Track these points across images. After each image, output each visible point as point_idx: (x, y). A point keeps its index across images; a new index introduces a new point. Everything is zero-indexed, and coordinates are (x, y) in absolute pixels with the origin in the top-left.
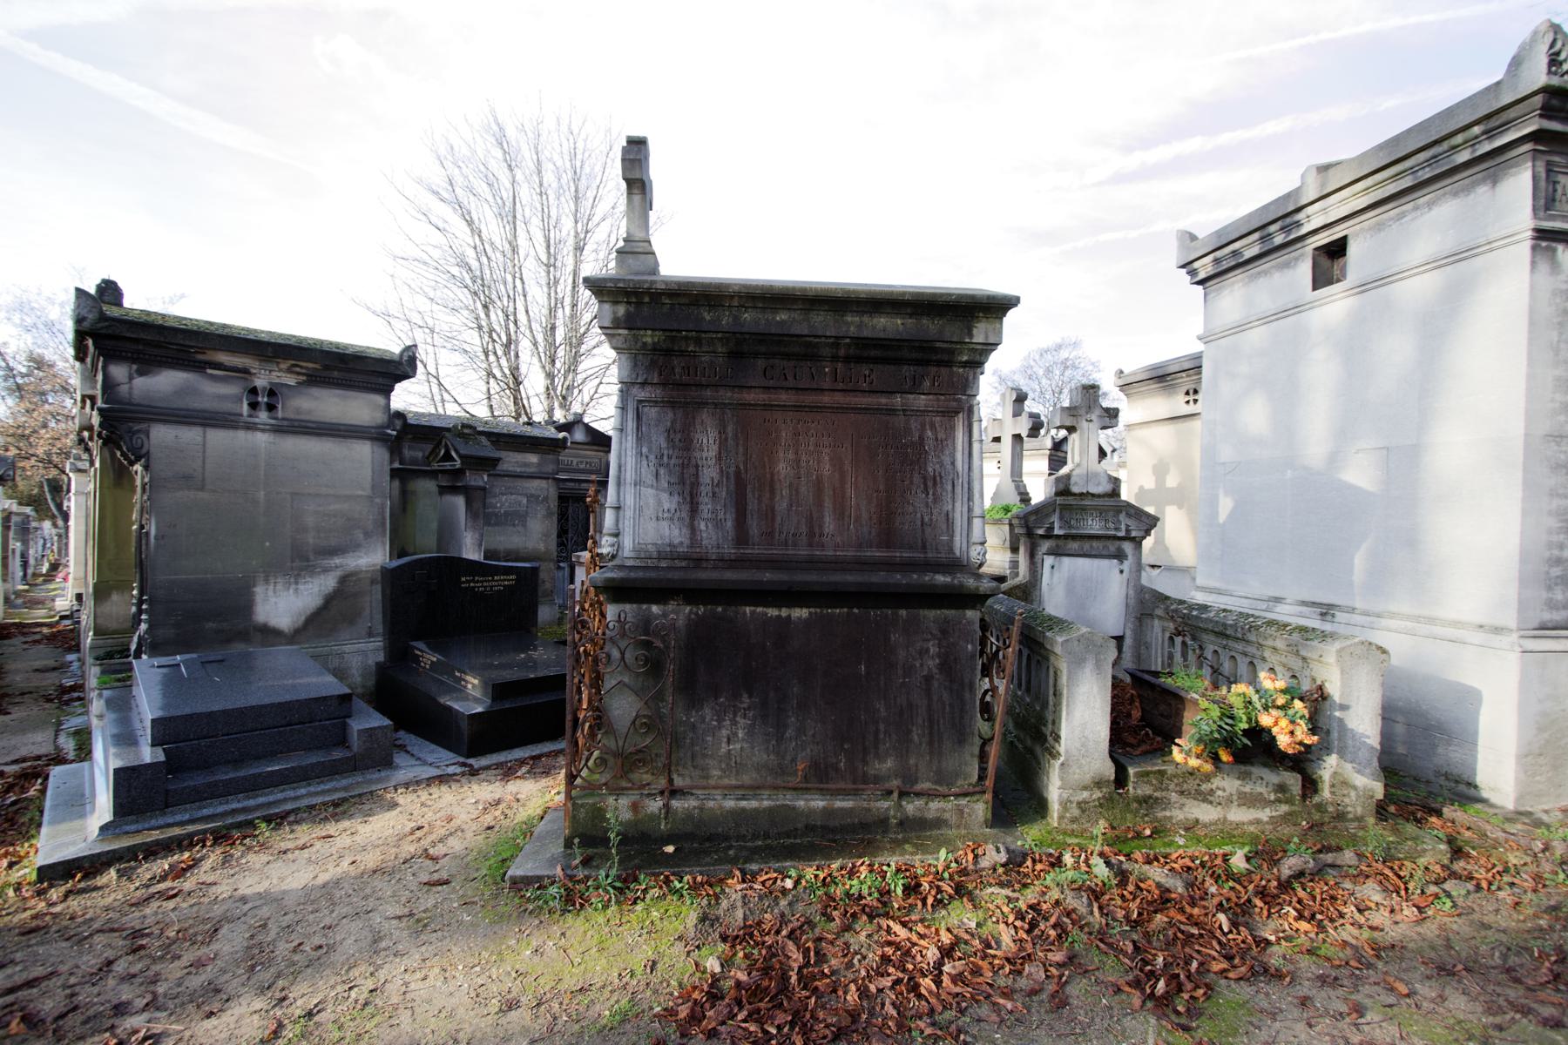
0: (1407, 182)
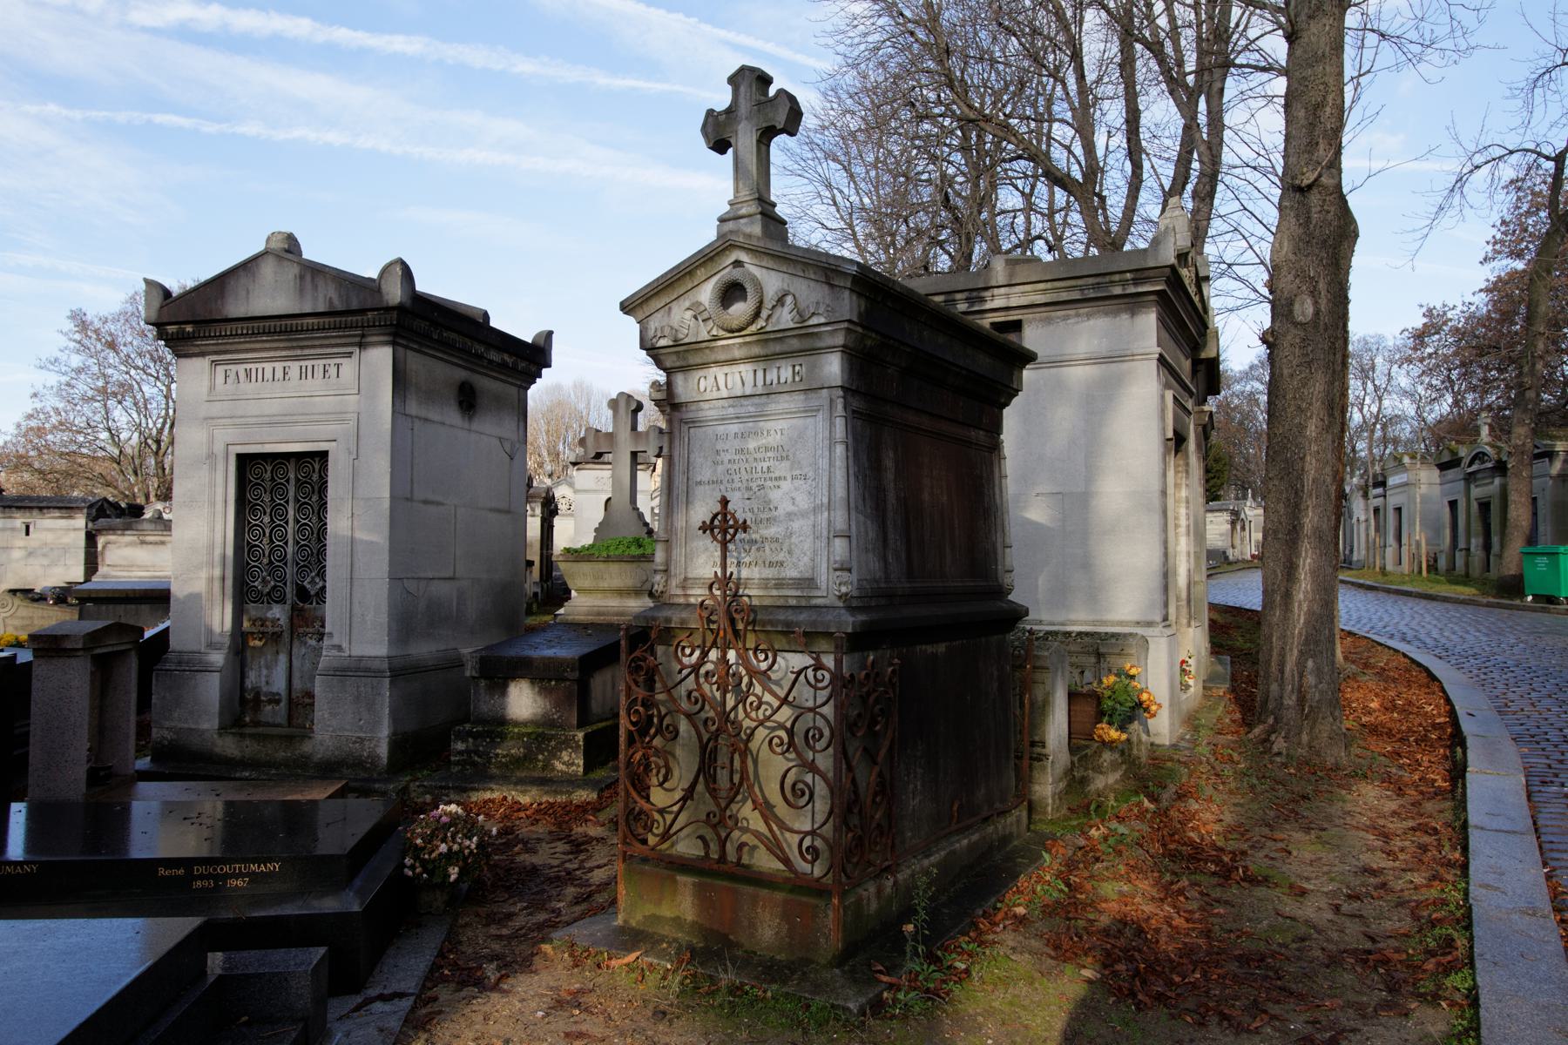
0: (1076, 295)
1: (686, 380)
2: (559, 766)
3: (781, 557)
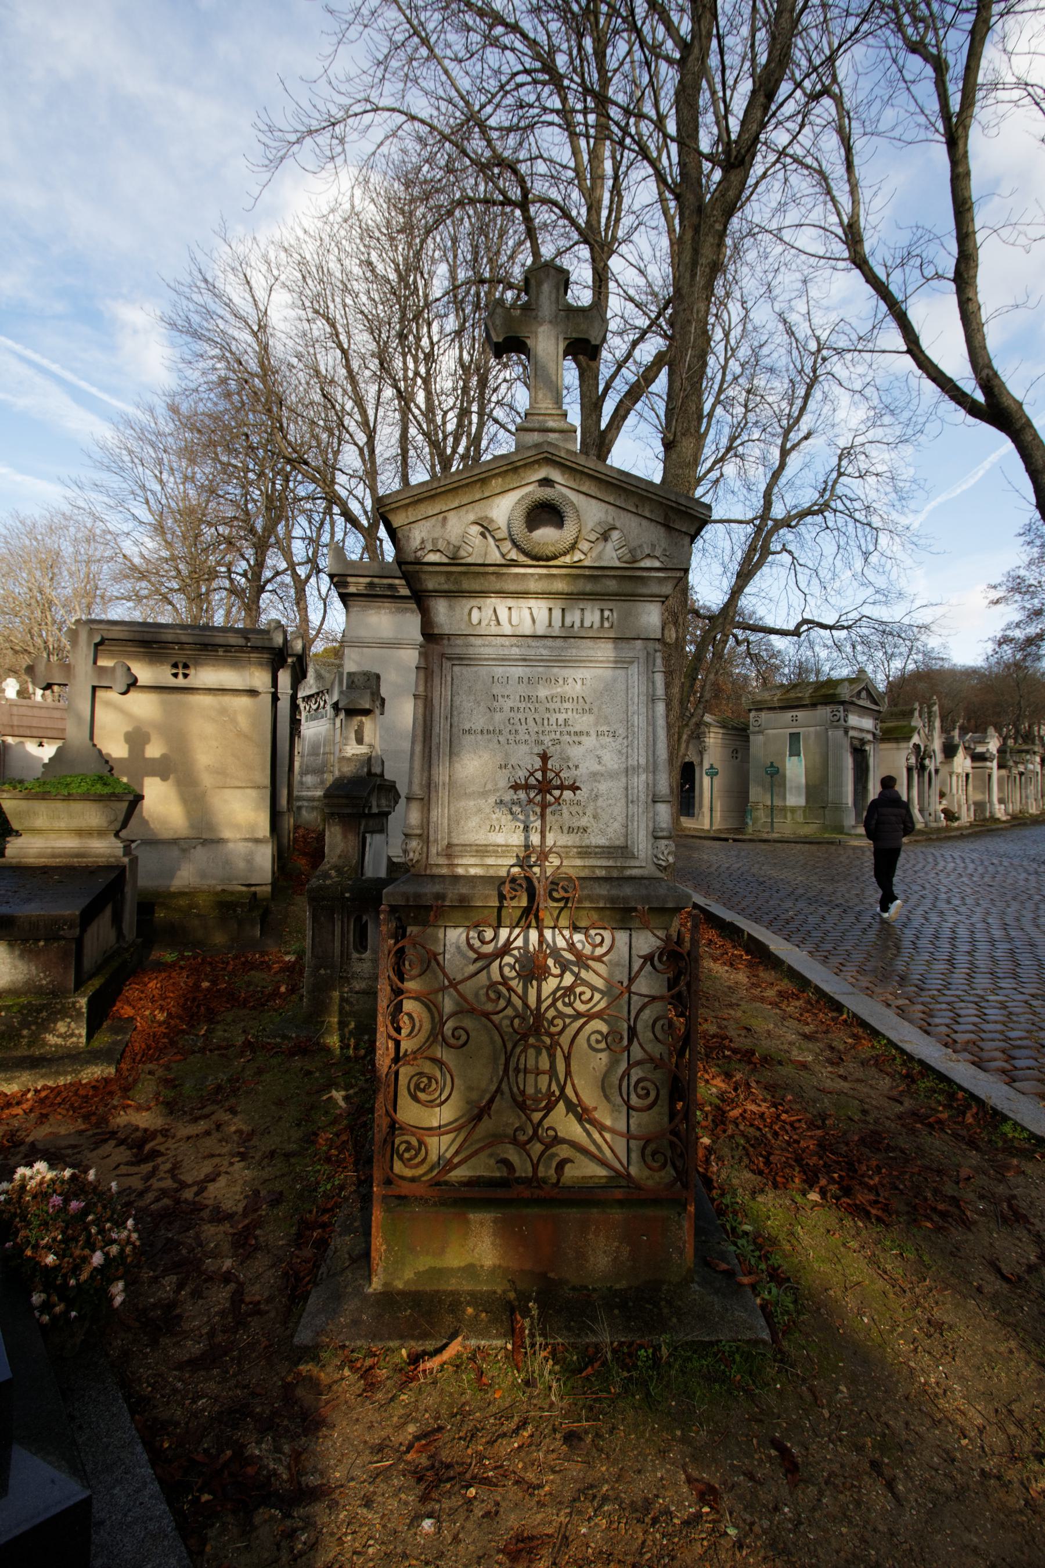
1: (451, 608)
2: (51, 1039)
3: (584, 822)
